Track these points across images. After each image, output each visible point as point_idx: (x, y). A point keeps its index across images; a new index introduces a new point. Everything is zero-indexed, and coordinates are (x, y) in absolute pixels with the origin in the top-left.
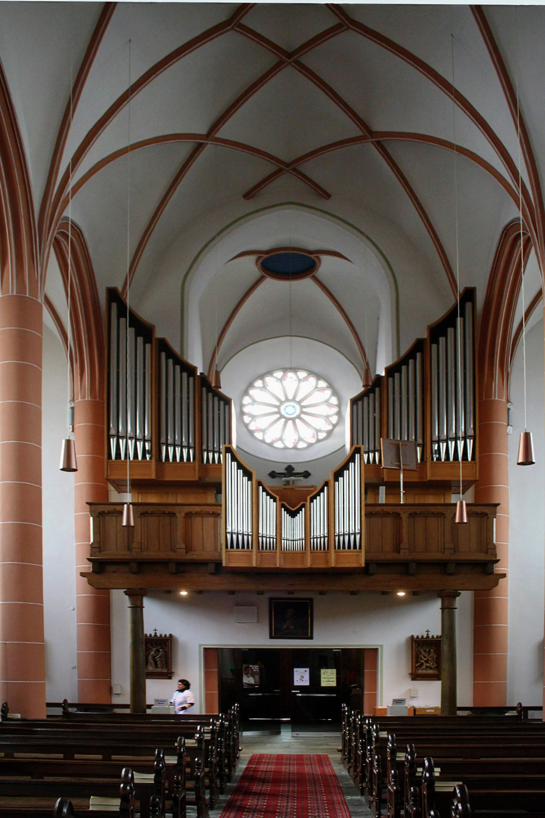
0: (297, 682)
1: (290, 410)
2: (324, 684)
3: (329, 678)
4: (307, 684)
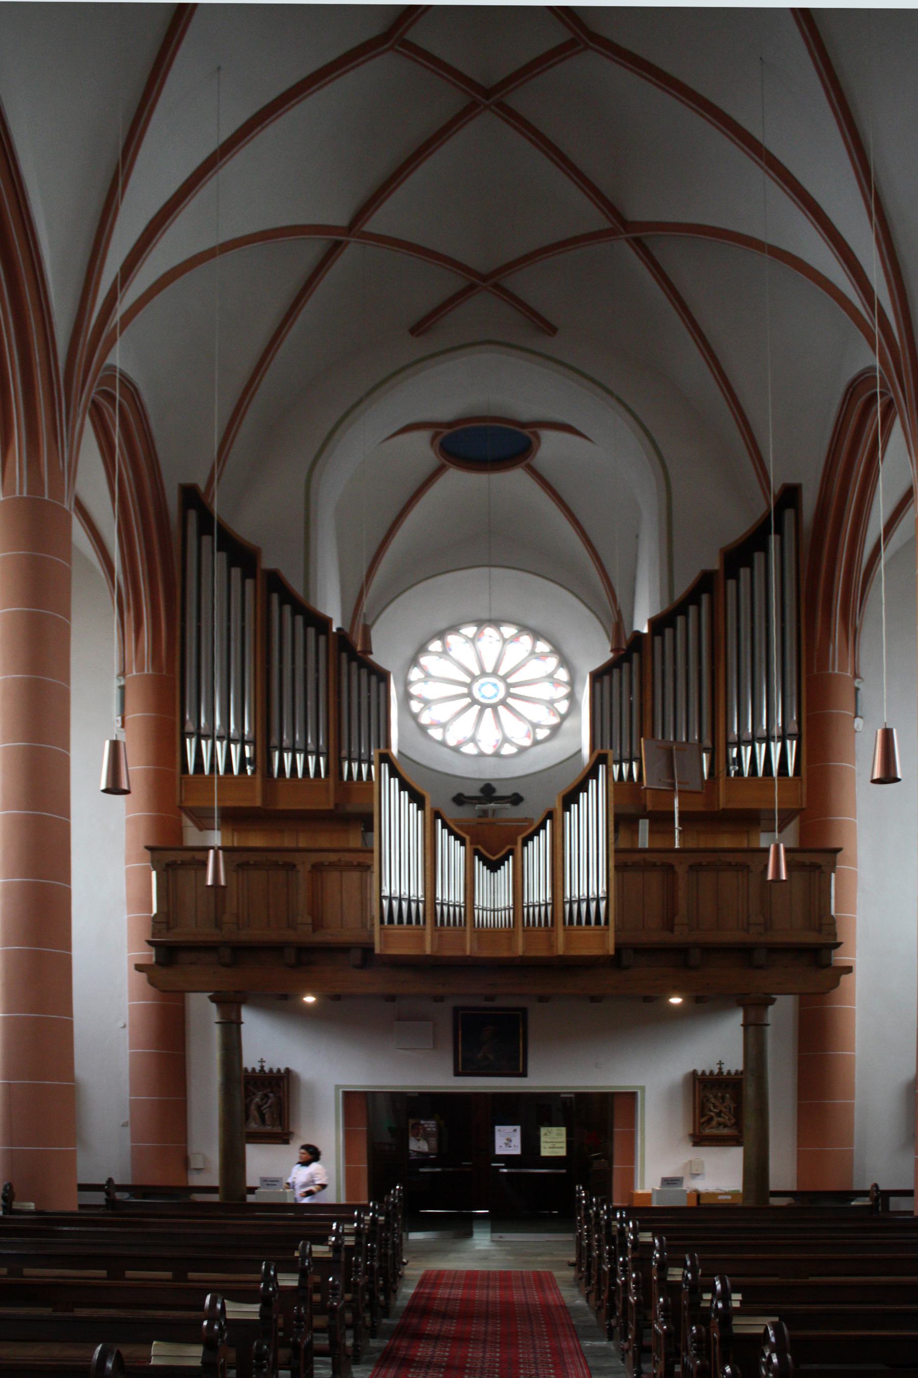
0: (501, 1149)
1: (489, 690)
2: (545, 1152)
3: (553, 1142)
4: (518, 1151)
